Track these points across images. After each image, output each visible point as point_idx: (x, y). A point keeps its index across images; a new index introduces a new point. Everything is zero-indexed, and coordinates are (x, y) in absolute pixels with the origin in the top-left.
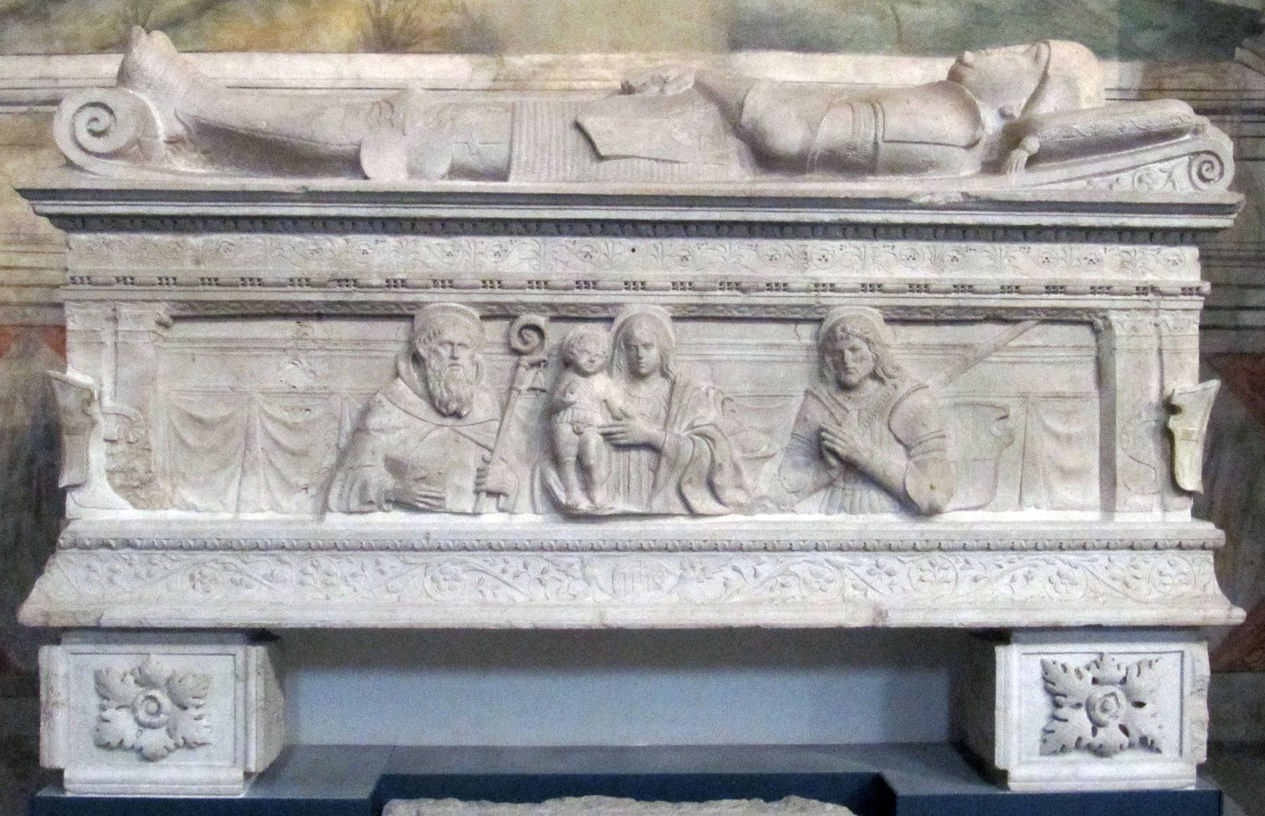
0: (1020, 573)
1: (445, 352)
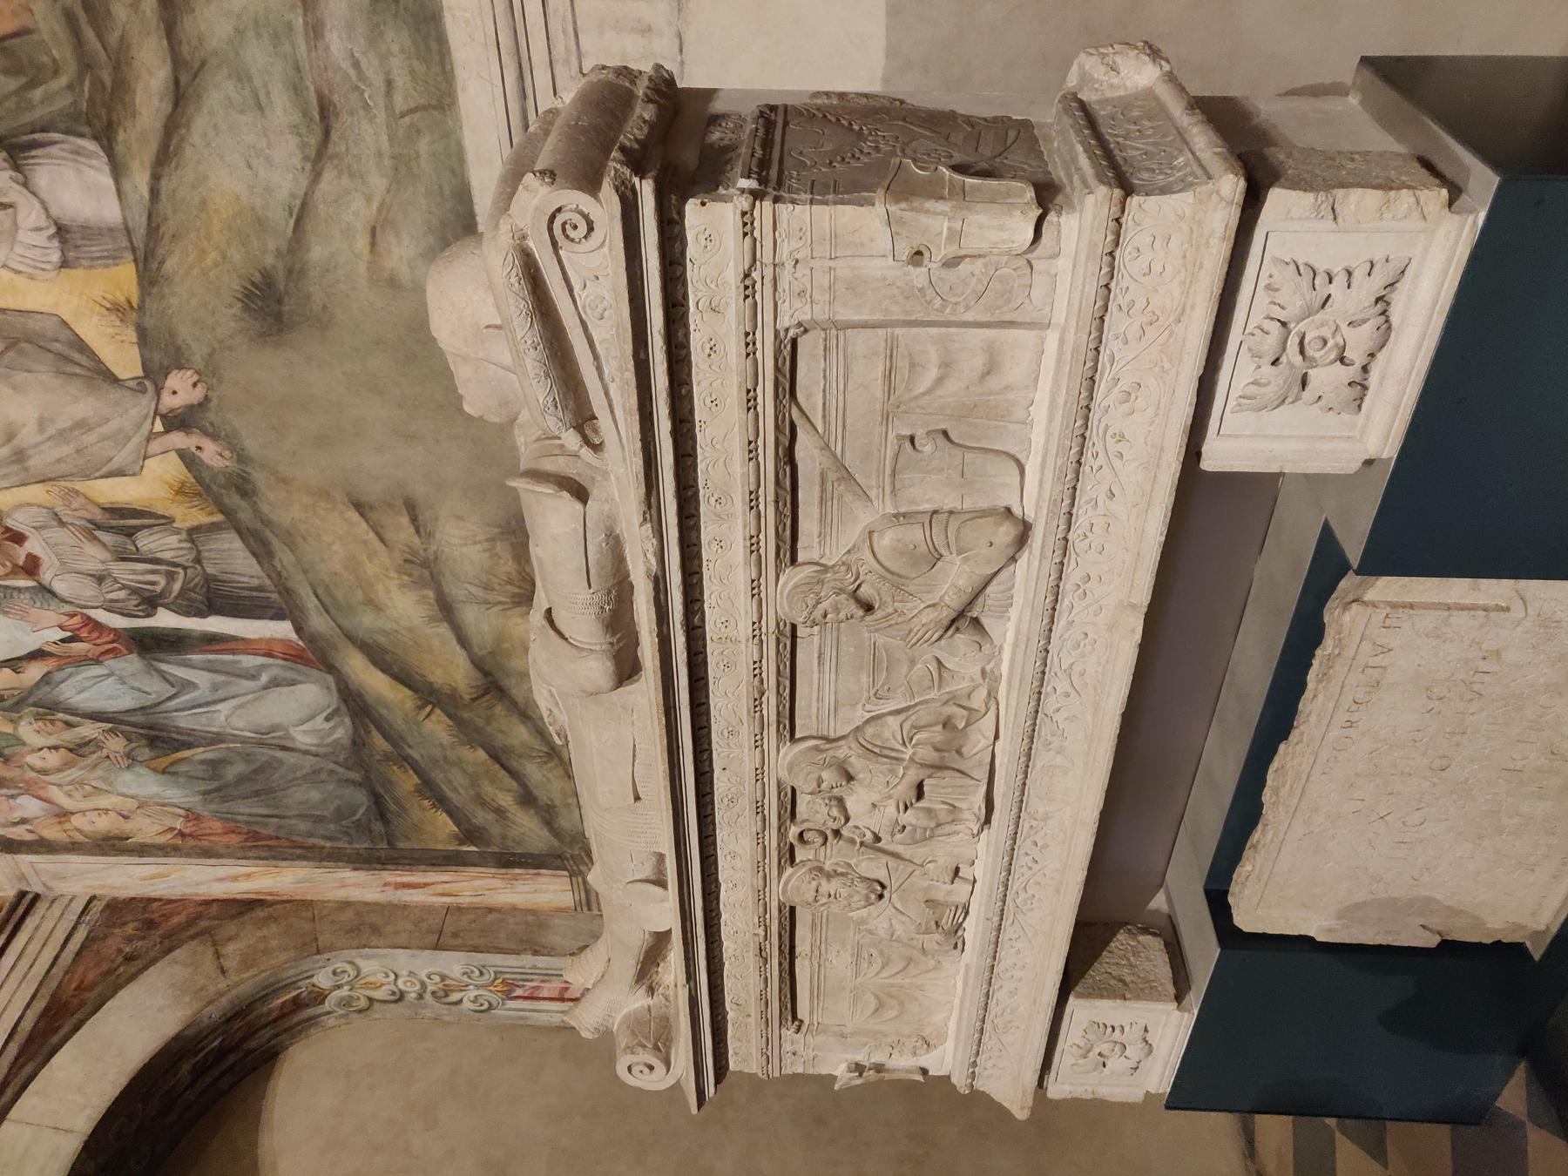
0: (1112, 446)
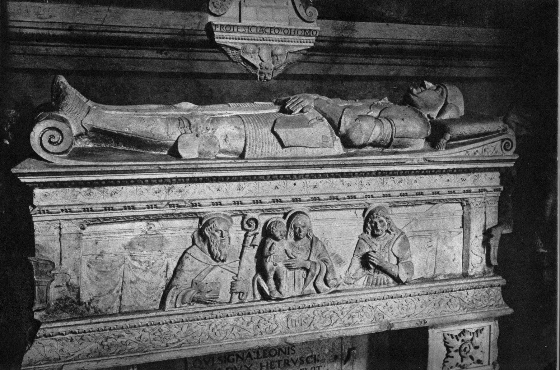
1: (218, 234)
